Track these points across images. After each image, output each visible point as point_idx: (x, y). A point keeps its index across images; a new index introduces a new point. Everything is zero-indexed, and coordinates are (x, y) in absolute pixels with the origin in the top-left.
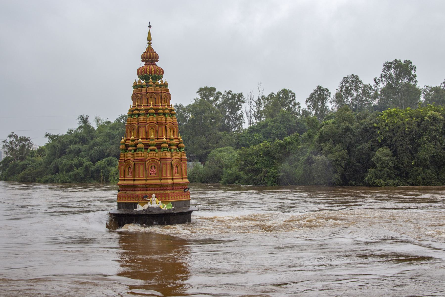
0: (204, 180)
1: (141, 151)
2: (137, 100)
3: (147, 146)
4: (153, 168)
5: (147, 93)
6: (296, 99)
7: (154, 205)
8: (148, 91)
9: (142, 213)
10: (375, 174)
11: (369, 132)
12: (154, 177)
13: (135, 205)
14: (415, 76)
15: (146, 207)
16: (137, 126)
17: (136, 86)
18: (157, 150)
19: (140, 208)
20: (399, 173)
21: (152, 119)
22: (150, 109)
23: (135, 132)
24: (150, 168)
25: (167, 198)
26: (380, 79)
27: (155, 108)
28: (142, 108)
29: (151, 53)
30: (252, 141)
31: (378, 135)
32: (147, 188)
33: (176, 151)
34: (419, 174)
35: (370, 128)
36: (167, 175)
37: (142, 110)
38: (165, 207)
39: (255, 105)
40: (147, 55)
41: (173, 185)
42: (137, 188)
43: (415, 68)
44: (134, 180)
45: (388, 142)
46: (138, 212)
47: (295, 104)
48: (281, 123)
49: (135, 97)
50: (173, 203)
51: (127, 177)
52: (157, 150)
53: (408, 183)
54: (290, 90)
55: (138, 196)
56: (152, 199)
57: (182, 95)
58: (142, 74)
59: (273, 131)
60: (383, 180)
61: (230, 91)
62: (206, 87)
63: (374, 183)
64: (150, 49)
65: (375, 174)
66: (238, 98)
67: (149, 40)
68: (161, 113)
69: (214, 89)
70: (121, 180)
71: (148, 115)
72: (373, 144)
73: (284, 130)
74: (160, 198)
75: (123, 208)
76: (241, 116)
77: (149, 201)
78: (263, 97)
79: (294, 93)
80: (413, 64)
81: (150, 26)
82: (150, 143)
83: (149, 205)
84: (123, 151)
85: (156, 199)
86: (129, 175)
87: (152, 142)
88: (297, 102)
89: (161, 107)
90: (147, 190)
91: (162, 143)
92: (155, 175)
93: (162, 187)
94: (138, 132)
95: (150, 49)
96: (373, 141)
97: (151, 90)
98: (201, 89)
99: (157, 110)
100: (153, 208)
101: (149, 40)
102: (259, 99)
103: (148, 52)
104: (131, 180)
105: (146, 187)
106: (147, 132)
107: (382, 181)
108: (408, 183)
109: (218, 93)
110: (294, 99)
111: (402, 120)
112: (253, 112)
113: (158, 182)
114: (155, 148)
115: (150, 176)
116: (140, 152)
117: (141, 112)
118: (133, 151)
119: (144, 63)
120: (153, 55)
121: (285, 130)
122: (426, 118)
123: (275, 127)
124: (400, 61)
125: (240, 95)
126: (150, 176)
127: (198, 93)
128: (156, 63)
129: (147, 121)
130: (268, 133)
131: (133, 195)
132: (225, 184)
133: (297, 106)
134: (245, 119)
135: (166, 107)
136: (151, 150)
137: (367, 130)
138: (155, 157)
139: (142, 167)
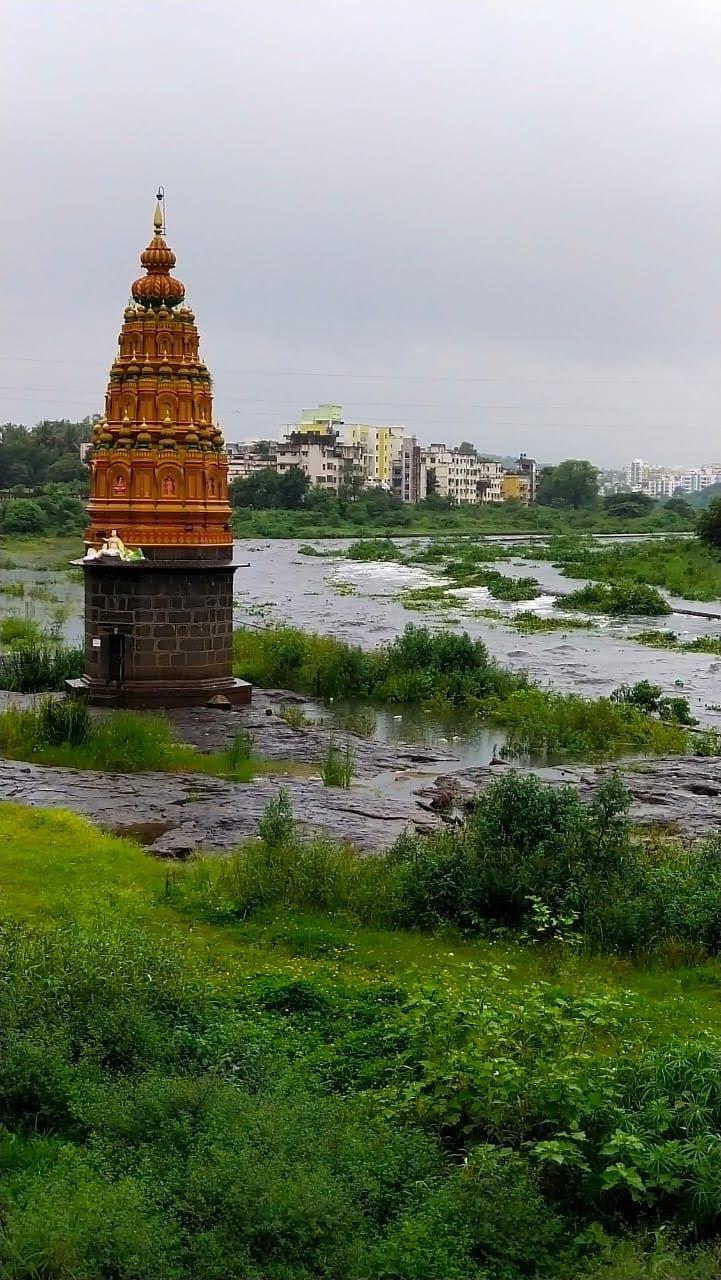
2: (134, 345)
7: (112, 552)
18: (177, 447)
20: (573, 521)
21: (167, 385)
22: (130, 365)
23: (132, 408)
24: (163, 483)
28: (147, 361)
29: (163, 252)
36: (196, 495)
37: (147, 365)
38: (129, 556)
41: (206, 515)
42: (136, 518)
49: (127, 340)
50: (146, 551)
56: (111, 539)
58: (141, 294)
64: (158, 245)
82: (163, 431)
83: (104, 550)
84: (107, 446)
87: (169, 431)
89: (184, 362)
91: (186, 434)
92: (122, 494)
93: (132, 517)
94: (138, 409)
95: (158, 245)
97: (165, 327)
103: (156, 249)
106: (156, 410)
113: (125, 507)
117: (145, 369)
118: (128, 446)
120: (167, 254)
135: (193, 361)
136: (167, 446)
138: (166, 461)
139: (147, 479)
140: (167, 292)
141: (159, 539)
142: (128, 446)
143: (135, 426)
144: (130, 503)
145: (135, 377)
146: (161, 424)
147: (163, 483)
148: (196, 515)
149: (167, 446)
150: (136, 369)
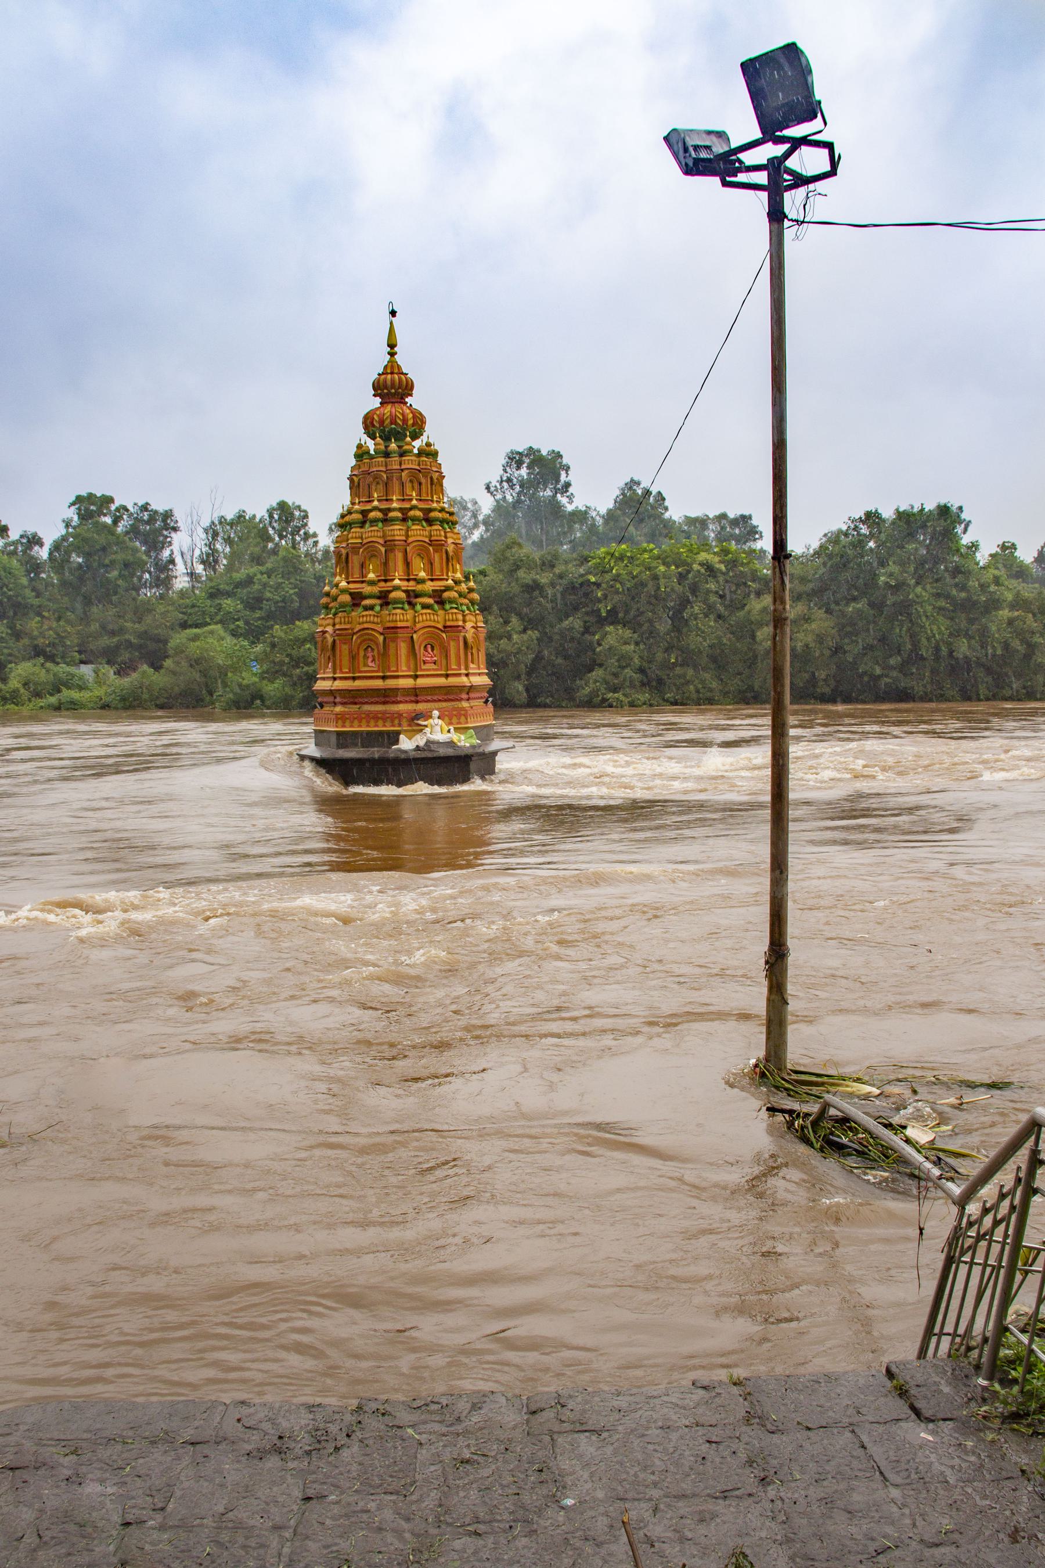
0: (162, 700)
1: (402, 608)
3: (412, 596)
4: (430, 650)
5: (402, 470)
6: (309, 524)
7: (440, 737)
8: (403, 467)
9: (412, 755)
10: (607, 683)
11: (578, 595)
12: (434, 670)
13: (394, 738)
14: (568, 485)
15: (420, 740)
16: (383, 549)
17: (361, 454)
19: (406, 744)
21: (419, 532)
22: (411, 509)
25: (463, 719)
26: (498, 485)
27: (384, 506)
28: (395, 505)
29: (396, 376)
30: (218, 618)
31: (599, 601)
32: (417, 696)
33: (433, 609)
34: (688, 682)
35: (581, 584)
37: (394, 510)
39: (204, 536)
40: (385, 380)
43: (567, 469)
44: (416, 677)
45: (621, 615)
46: (405, 752)
47: (307, 537)
48: (283, 577)
49: (356, 485)
51: (422, 670)
52: (436, 607)
53: (667, 701)
54: (297, 504)
55: (400, 715)
56: (431, 721)
57: (471, 479)
59: (268, 595)
60: (624, 695)
61: (147, 504)
62: (91, 495)
63: (604, 700)
64: (392, 368)
65: (607, 683)
66: (164, 520)
67: (392, 345)
68: (437, 519)
69: (111, 500)
70: (341, 678)
71: (410, 523)
72: (587, 618)
73: (291, 592)
74: (446, 719)
75: (356, 745)
76: (172, 561)
77: (426, 726)
78: (222, 521)
79: (305, 511)
80: (565, 462)
81: (393, 313)
82: (419, 587)
85: (440, 722)
86: (366, 665)
88: (311, 532)
90: (417, 702)
91: (445, 591)
95: (392, 368)
96: (587, 613)
98: (79, 499)
99: (386, 511)
100: (438, 743)
101: (392, 345)
102: (213, 523)
103: (387, 374)
104: (377, 677)
105: (415, 695)
106: (407, 564)
107: (622, 698)
108: (667, 701)
109: (118, 510)
110: (306, 525)
111: (649, 569)
112: (197, 553)
113: (441, 681)
114: (431, 601)
115: (424, 667)
116: (398, 611)
118: (378, 608)
119: (378, 400)
120: (400, 380)
121: (295, 593)
122: (696, 567)
123: (271, 587)
124: (539, 451)
125: (168, 515)
126: (424, 667)
127: (73, 508)
128: (409, 400)
129: (407, 536)
130: (253, 598)
131: (384, 713)
132: (230, 709)
133: (311, 541)
134: (180, 568)
136: (425, 606)
137: (573, 588)
138: (433, 624)
140: (411, 422)
141: (347, 723)
142: (378, 608)
143: (382, 584)
144: (384, 678)
145: (380, 524)
146: (415, 580)
147: (362, 653)
148: (461, 688)
149: (425, 606)
150: (379, 515)
